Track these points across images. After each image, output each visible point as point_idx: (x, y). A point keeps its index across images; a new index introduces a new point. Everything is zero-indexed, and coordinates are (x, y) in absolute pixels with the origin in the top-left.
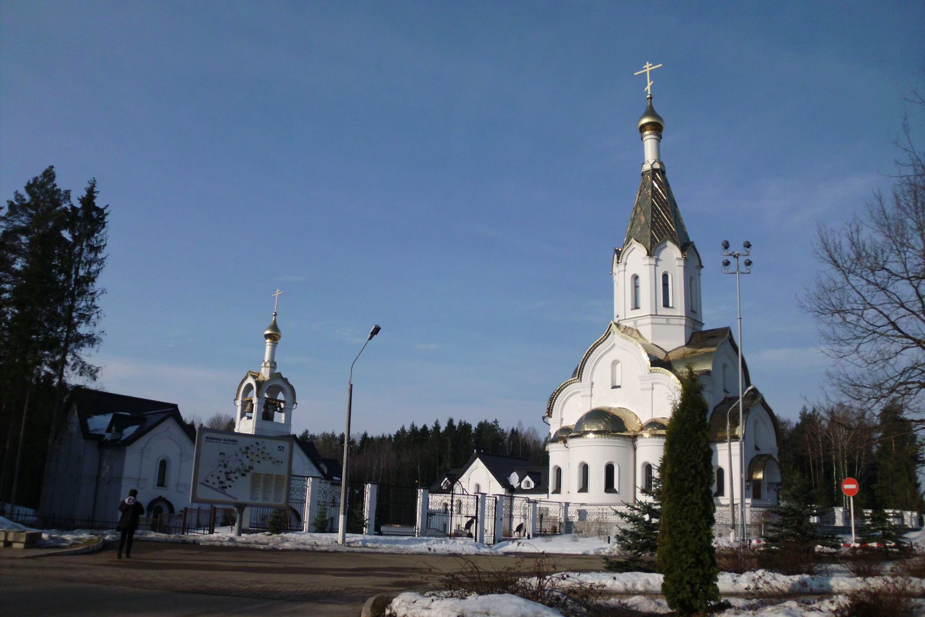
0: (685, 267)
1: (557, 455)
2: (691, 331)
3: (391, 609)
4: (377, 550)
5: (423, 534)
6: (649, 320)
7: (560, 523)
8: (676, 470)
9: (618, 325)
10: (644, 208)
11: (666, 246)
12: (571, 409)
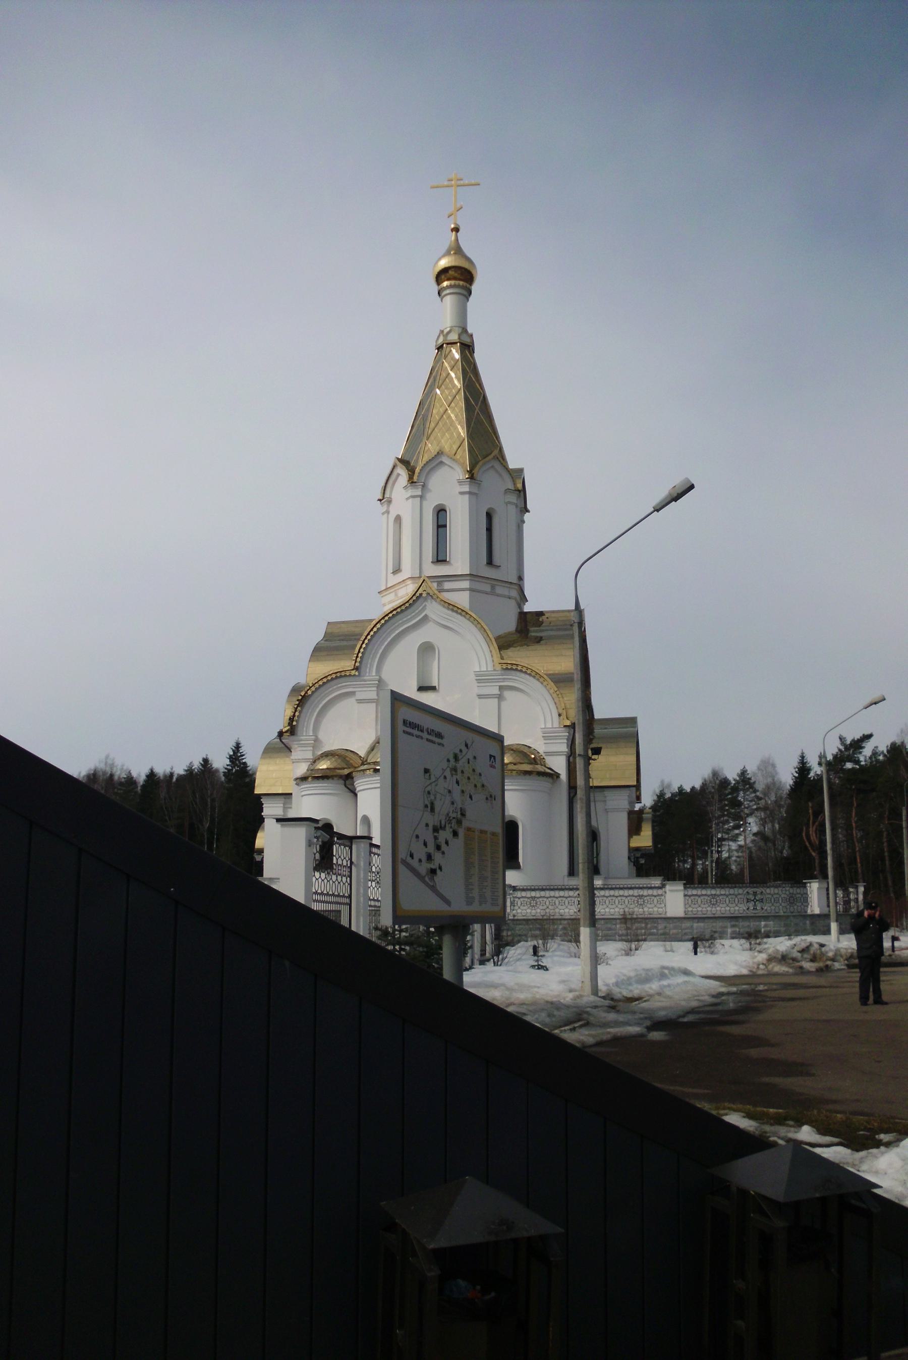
4: (720, 1008)
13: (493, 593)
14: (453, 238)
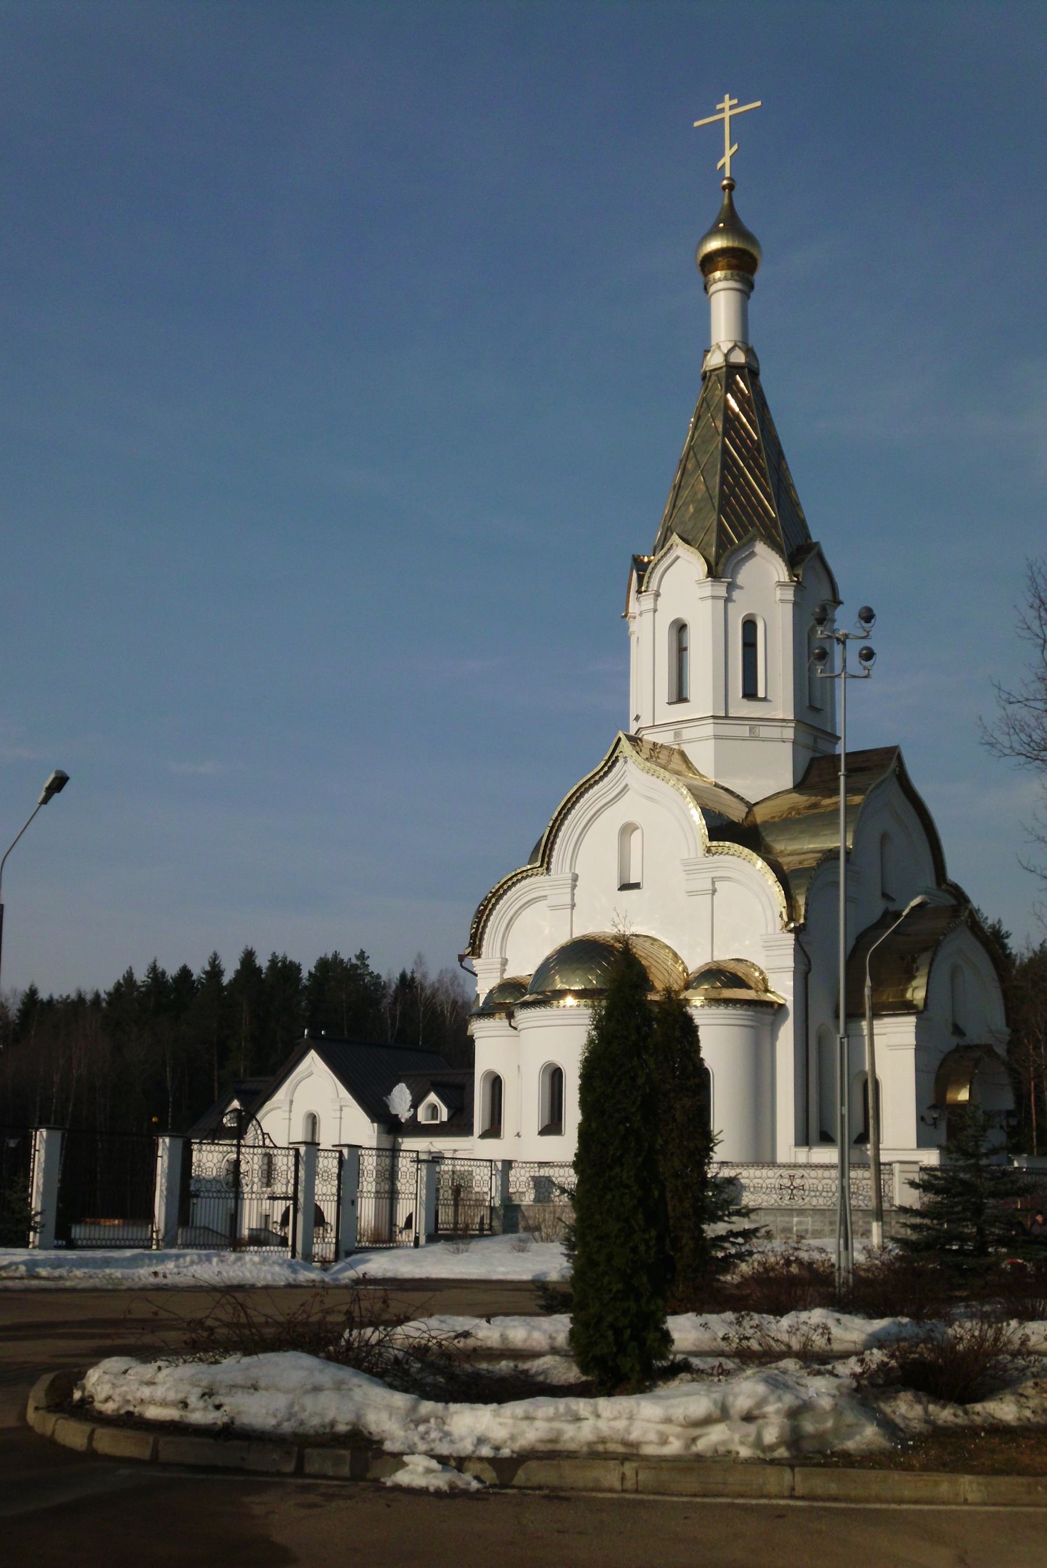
0: (796, 604)
1: (493, 1046)
2: (806, 756)
3: (83, 1389)
4: (61, 1284)
5: (170, 1241)
6: (708, 729)
7: (492, 1209)
8: (594, 1125)
9: (634, 740)
10: (704, 460)
11: (752, 554)
12: (525, 938)
13: (754, 737)
14: (726, 201)
